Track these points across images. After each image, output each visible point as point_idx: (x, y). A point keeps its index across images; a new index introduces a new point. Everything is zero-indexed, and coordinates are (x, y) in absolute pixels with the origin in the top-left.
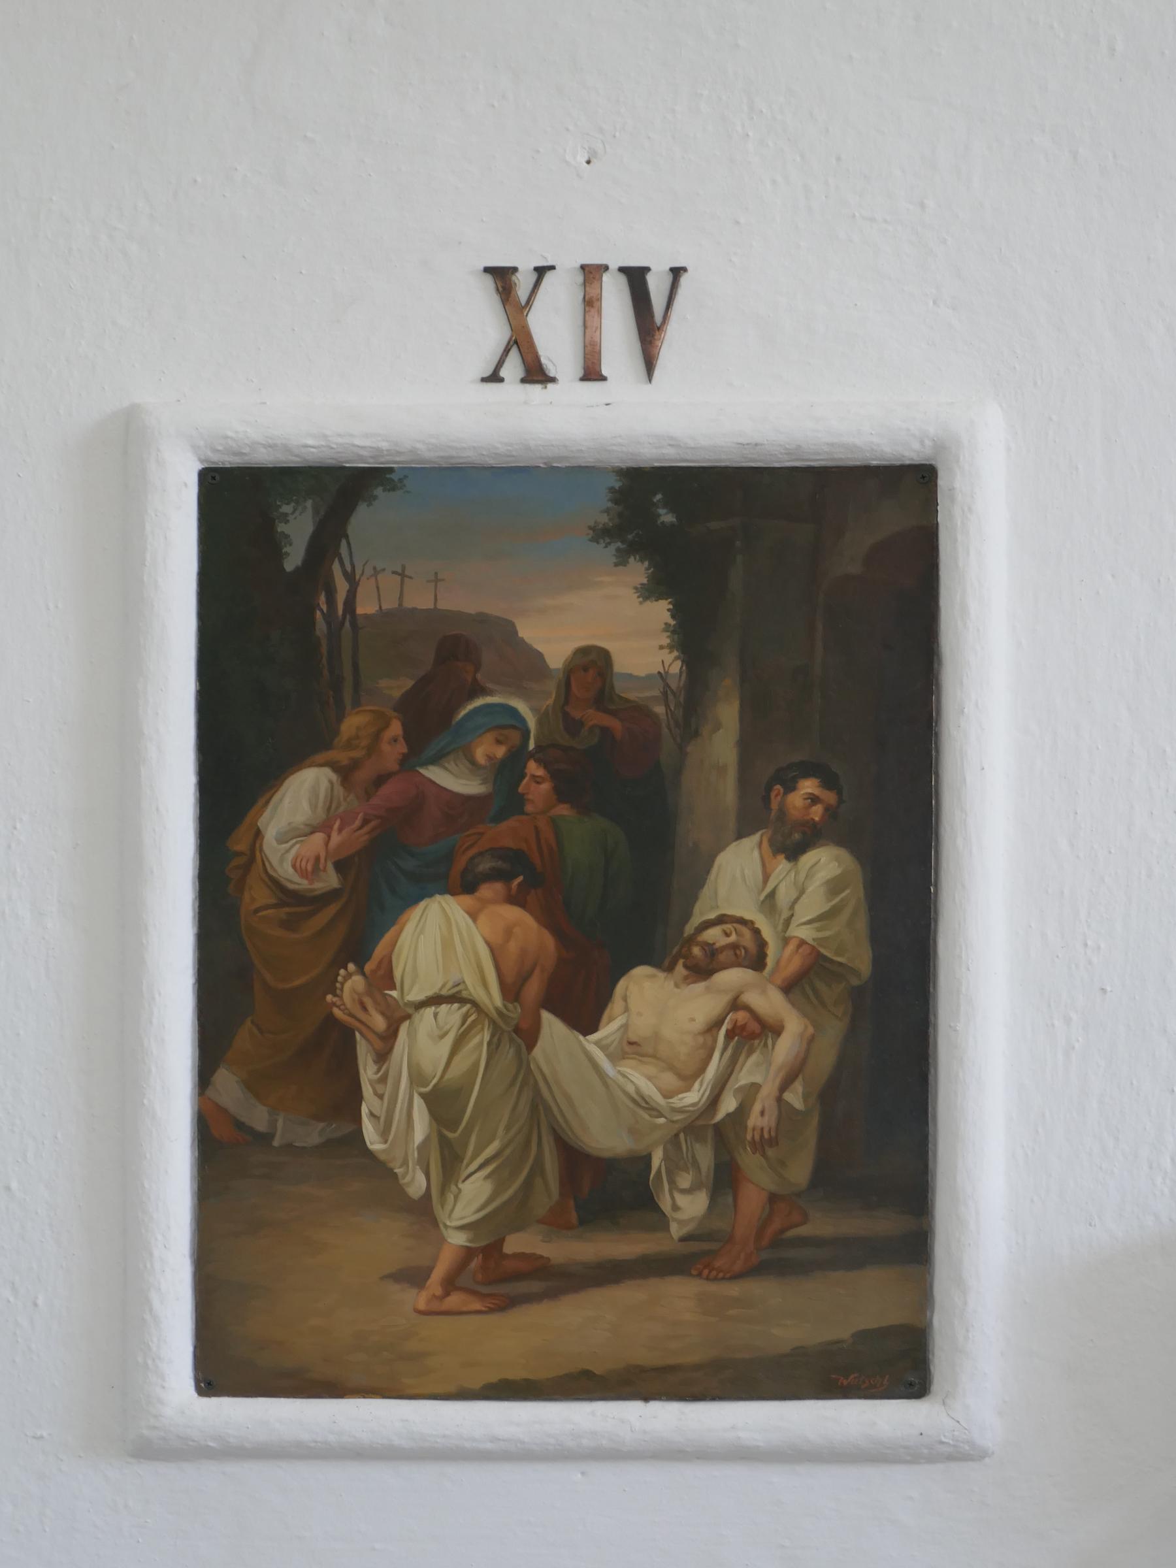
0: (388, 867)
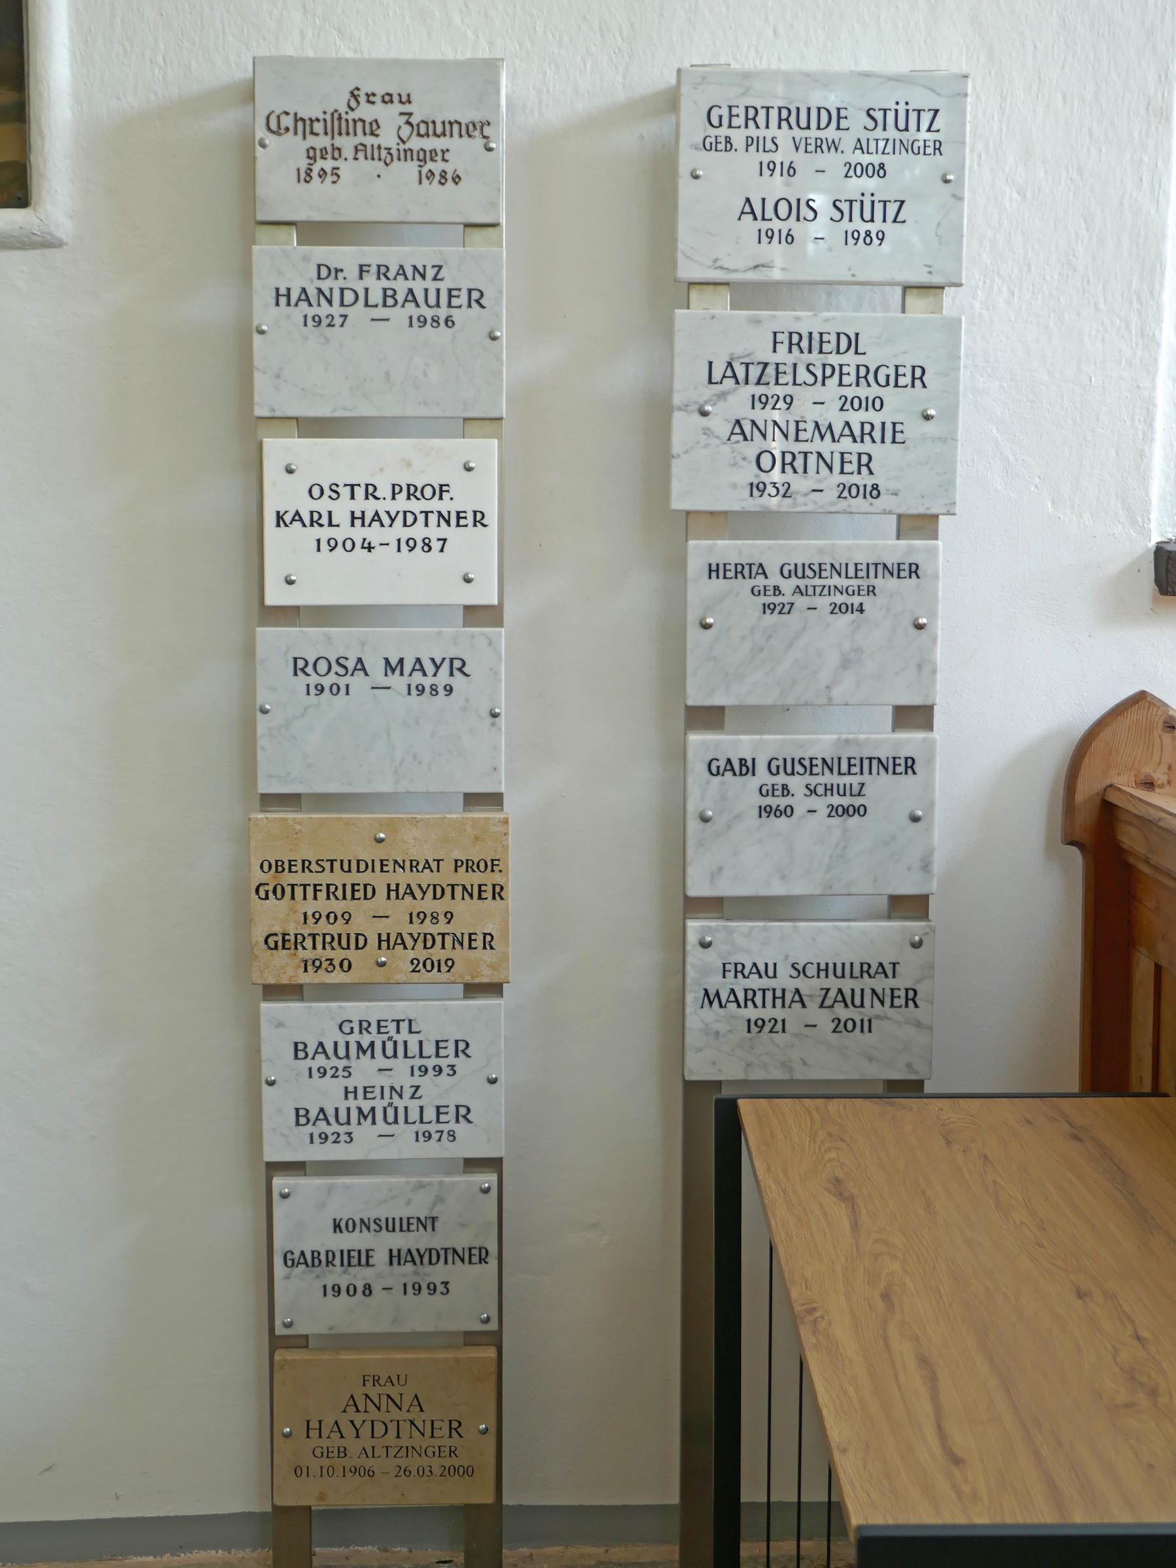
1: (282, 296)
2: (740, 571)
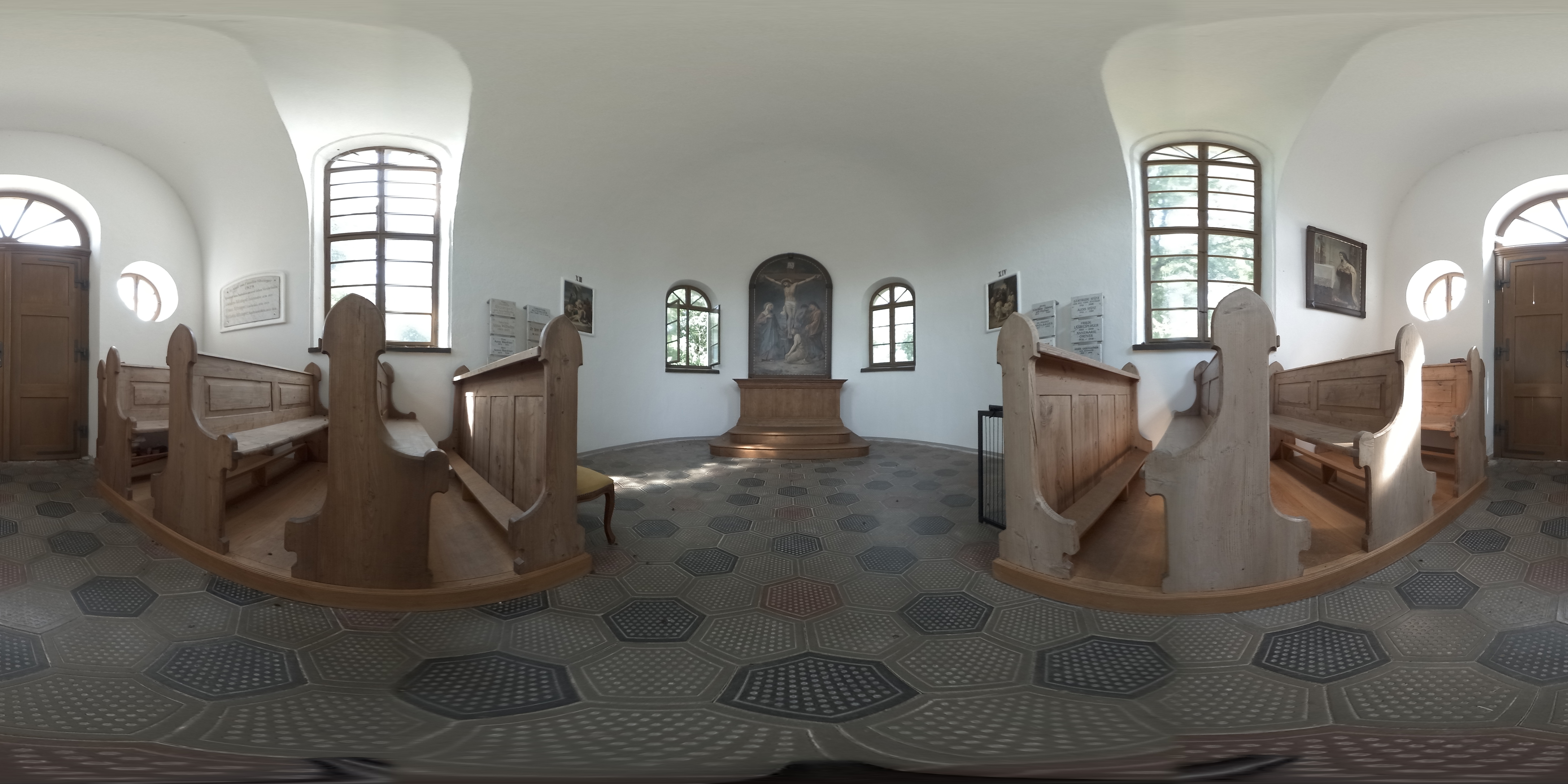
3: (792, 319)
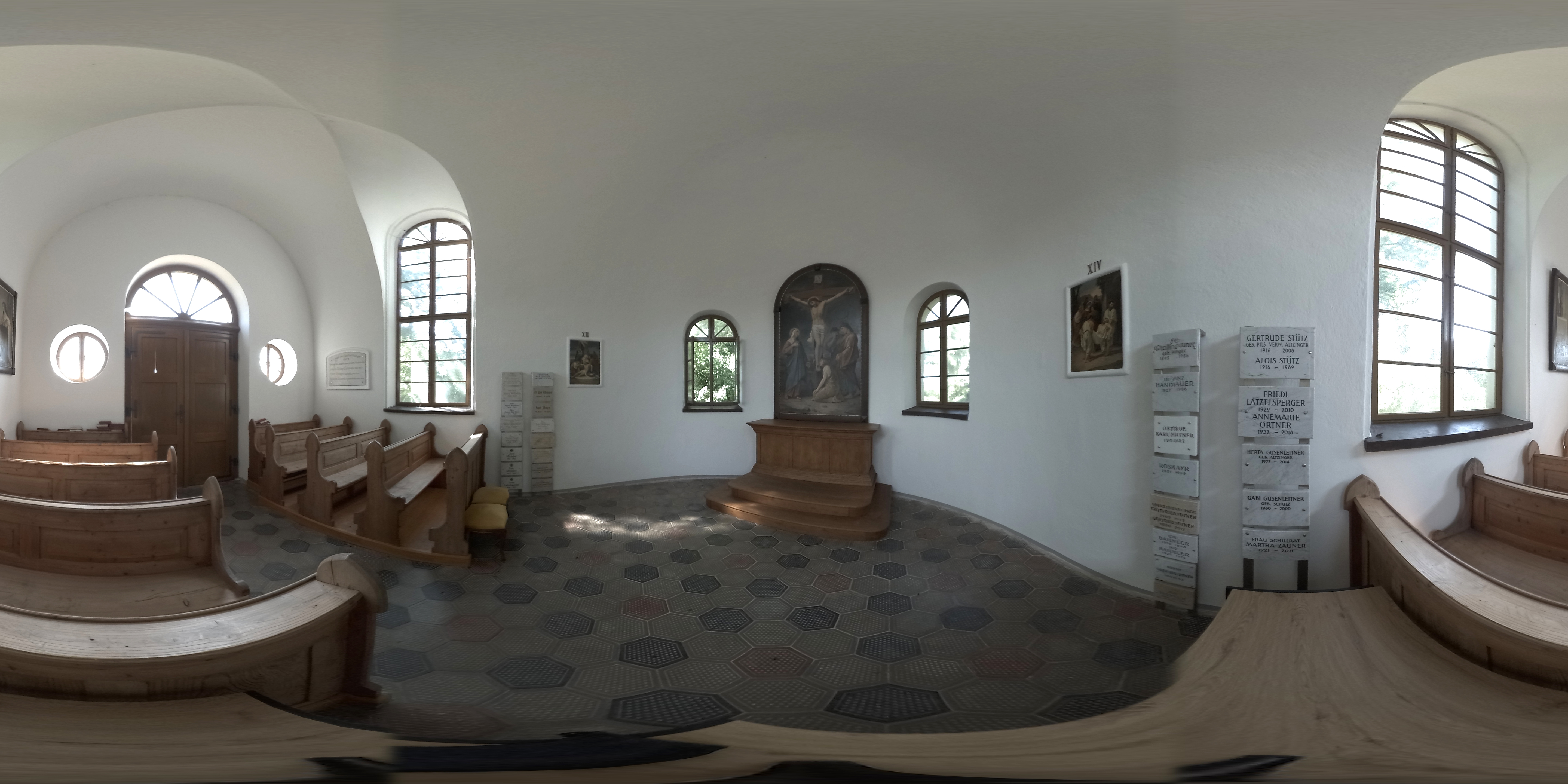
0: (1082, 320)
1: (1158, 385)
2: (1256, 452)
3: (820, 347)
